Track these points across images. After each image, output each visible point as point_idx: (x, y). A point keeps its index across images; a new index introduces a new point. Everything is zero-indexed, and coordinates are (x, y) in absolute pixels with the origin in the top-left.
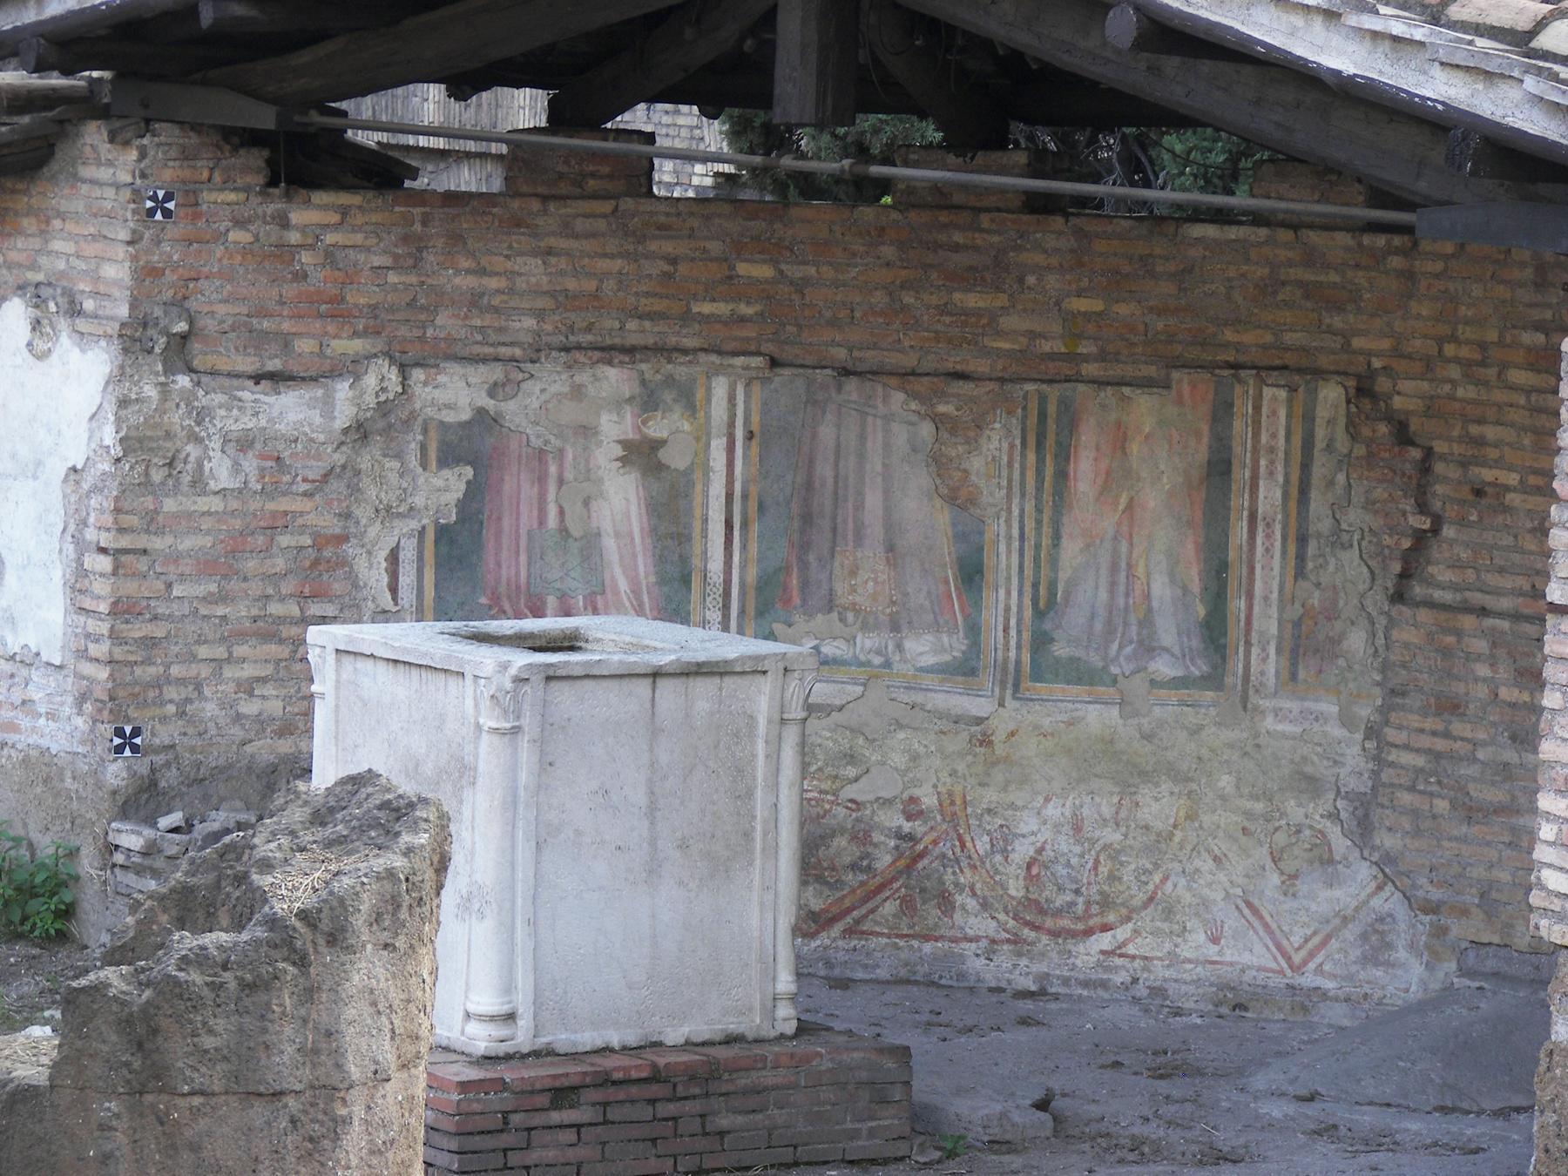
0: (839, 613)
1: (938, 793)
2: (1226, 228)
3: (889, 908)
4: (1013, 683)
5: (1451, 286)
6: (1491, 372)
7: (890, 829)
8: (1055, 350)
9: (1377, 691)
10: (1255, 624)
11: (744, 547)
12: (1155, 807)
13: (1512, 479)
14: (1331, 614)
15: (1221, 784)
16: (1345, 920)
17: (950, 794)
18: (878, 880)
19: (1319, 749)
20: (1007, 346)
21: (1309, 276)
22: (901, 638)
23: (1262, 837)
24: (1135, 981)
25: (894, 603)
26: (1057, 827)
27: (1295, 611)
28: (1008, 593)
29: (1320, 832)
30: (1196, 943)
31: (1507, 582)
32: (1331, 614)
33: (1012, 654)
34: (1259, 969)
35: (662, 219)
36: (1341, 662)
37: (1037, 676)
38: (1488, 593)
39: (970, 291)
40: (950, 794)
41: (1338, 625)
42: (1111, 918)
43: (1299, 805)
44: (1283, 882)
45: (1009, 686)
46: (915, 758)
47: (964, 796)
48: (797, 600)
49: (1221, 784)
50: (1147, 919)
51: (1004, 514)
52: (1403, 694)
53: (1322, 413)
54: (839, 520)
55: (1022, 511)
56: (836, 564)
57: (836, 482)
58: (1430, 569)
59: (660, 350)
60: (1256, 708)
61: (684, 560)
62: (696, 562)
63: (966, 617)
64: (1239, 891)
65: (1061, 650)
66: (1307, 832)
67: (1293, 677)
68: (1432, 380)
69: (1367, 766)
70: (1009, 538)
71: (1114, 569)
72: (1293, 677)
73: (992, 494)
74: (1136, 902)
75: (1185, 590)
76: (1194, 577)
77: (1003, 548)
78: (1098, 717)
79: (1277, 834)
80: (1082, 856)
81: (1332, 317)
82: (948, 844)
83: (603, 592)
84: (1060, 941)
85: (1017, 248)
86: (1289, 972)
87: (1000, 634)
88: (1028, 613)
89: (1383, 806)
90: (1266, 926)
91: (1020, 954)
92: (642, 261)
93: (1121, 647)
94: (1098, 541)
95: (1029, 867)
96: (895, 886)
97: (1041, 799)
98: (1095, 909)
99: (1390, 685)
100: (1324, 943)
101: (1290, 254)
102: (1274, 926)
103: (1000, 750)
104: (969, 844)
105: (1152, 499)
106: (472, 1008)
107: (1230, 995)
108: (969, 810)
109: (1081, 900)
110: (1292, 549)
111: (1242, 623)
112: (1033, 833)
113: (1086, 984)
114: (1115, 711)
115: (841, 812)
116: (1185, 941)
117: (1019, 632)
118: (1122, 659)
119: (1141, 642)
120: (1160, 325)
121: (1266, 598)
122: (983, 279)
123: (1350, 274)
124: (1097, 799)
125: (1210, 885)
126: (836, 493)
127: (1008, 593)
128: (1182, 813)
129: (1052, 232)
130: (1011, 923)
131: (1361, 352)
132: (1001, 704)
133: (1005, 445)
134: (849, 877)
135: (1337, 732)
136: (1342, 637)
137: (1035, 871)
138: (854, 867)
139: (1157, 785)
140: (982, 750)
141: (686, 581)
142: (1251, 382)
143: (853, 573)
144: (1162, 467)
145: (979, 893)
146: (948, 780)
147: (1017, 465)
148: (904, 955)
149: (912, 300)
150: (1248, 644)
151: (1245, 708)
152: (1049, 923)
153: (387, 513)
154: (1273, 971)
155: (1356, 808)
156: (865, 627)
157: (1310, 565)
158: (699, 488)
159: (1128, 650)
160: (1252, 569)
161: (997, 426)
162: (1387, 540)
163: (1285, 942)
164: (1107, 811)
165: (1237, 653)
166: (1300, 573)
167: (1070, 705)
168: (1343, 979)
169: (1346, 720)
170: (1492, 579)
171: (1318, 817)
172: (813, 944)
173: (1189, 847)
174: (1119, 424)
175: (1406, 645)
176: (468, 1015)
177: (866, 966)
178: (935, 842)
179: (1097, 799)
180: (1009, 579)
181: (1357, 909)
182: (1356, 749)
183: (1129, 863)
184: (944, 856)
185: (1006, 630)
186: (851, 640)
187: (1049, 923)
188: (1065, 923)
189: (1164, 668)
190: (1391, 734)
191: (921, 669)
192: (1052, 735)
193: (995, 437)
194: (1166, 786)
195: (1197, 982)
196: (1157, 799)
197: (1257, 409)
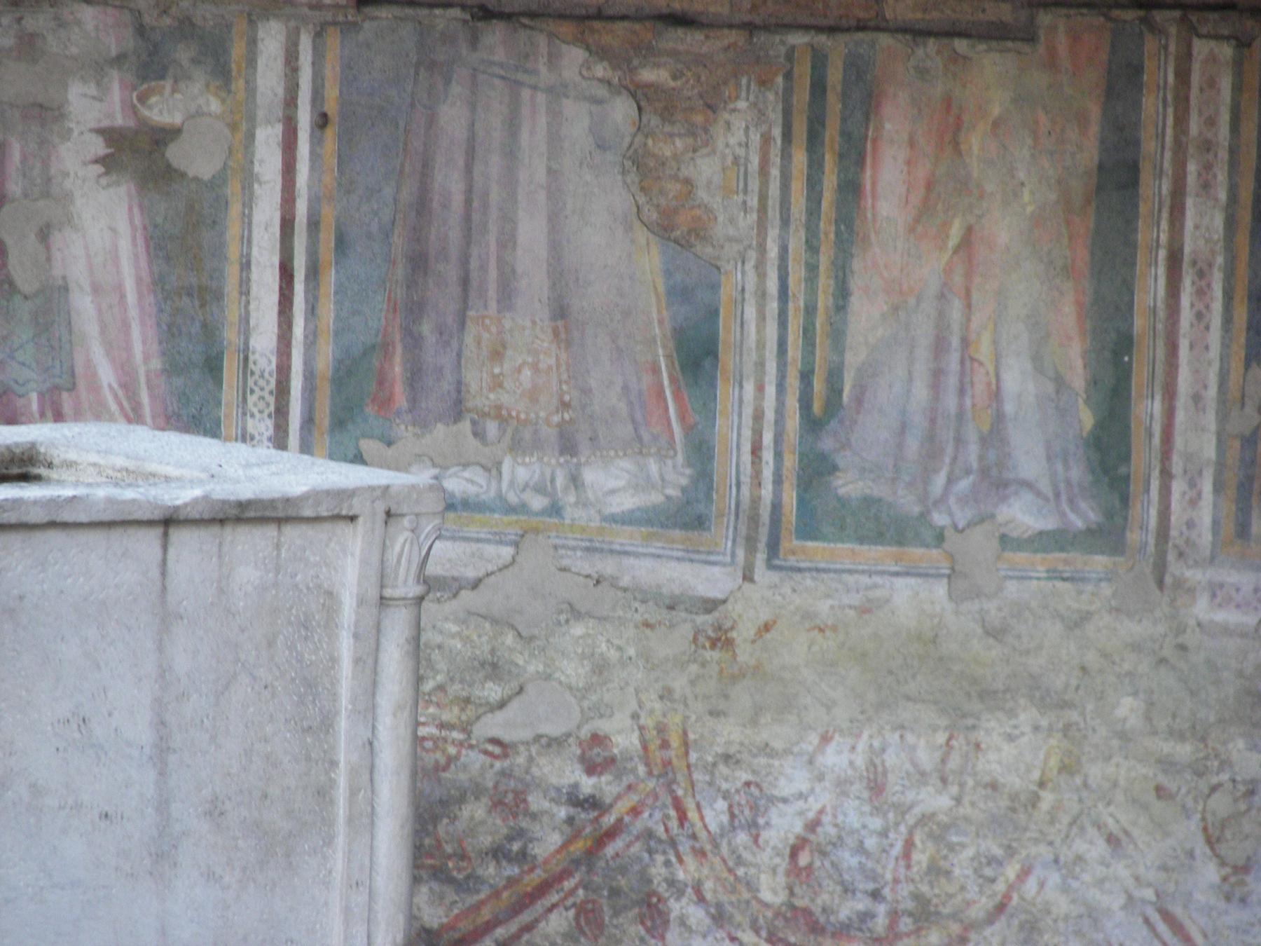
0: (474, 423)
1: (641, 728)
10: (1179, 442)
11: (312, 310)
12: (1008, 750)
15: (1121, 712)
17: (661, 729)
18: (538, 875)
22: (579, 465)
23: (1190, 802)
25: (565, 406)
26: (842, 786)
28: (760, 388)
33: (767, 492)
37: (808, 530)
40: (661, 729)
44: (1225, 879)
46: (601, 668)
47: (685, 733)
51: (752, 256)
54: (474, 264)
55: (784, 250)
56: (469, 339)
60: (1179, 584)
62: (230, 335)
63: (688, 429)
64: (1149, 894)
65: (848, 485)
70: (762, 295)
71: (940, 346)
72: (1243, 530)
73: (732, 221)
75: (1060, 383)
77: (750, 312)
80: (884, 834)
82: (658, 815)
83: (72, 388)
87: (747, 458)
88: (793, 422)
93: (950, 481)
95: (794, 853)
96: (568, 884)
97: (814, 738)
103: (745, 654)
104: (692, 815)
108: (693, 756)
109: (881, 909)
111: (1157, 440)
112: (801, 796)
115: (475, 760)
117: (778, 455)
118: (952, 500)
119: (984, 472)
124: (910, 739)
125: (1100, 882)
126: (467, 218)
127: (760, 388)
128: (1054, 762)
132: (748, 577)
133: (756, 138)
137: (804, 859)
138: (498, 853)
139: (1012, 713)
140: (717, 654)
141: (213, 367)
142: (1173, 30)
143: (497, 355)
144: (1022, 175)
145: (709, 896)
146: (658, 706)
147: (775, 172)
150: (1166, 475)
151: (1160, 583)
156: (516, 447)
158: (235, 209)
159: (964, 485)
160: (1173, 348)
161: (742, 104)
164: (927, 759)
165: (1148, 491)
167: (865, 580)
173: (1066, 820)
174: (948, 102)
178: (635, 811)
179: (910, 739)
180: (760, 365)
183: (963, 846)
184: (649, 834)
185: (756, 450)
186: (493, 468)
191: (613, 519)
192: (834, 629)
194: (1026, 717)
196: (1011, 738)
197: (1183, 76)
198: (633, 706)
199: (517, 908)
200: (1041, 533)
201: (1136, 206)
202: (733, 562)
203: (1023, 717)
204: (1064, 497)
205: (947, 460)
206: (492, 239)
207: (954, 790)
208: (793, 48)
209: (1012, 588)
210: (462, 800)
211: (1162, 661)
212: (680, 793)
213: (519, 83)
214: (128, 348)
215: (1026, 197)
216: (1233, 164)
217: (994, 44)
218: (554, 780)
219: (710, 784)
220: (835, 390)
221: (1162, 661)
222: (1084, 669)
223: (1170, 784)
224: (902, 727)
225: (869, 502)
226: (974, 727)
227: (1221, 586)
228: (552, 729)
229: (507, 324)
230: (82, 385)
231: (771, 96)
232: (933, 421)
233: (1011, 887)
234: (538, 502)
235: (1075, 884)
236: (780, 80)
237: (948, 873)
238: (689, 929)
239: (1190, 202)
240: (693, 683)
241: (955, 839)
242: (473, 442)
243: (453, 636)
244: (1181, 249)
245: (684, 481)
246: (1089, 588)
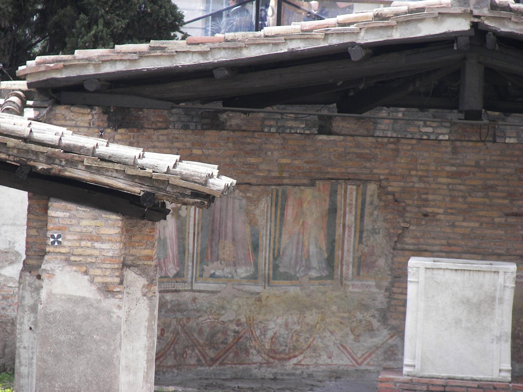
0: (220, 261)
1: (246, 317)
2: (330, 136)
3: (231, 355)
4: (268, 281)
5: (414, 154)
6: (431, 179)
7: (232, 330)
8: (276, 175)
9: (390, 277)
10: (345, 259)
11: (197, 241)
12: (311, 317)
13: (441, 211)
14: (372, 254)
15: (332, 309)
16: (377, 348)
17: (249, 317)
18: (229, 346)
19: (367, 296)
20: (262, 174)
21: (358, 151)
22: (236, 269)
23: (348, 325)
24: (302, 373)
25: (234, 257)
26: (280, 326)
27: (359, 254)
28: (266, 253)
29: (369, 321)
30: (324, 359)
31: (438, 242)
32: (372, 254)
33: (267, 272)
34: (345, 366)
35: (176, 135)
36: (376, 269)
37: (274, 279)
38: (429, 245)
39: (252, 157)
40: (249, 317)
41: (374, 258)
42: (297, 353)
43: (361, 313)
44: (355, 338)
45: (267, 282)
46: (240, 307)
47: (253, 318)
48: (209, 258)
49: (332, 309)
50: (308, 353)
51: (265, 228)
52: (399, 277)
53: (369, 193)
54: (221, 231)
55: (271, 226)
56: (220, 245)
57: (220, 219)
58: (404, 239)
60: (346, 285)
61: (184, 246)
62: (187, 247)
63: (254, 261)
64: (339, 342)
65: (282, 270)
66: (364, 322)
67: (358, 274)
68: (404, 182)
69: (385, 300)
70: (266, 235)
71: (298, 243)
72: (358, 274)
73: (262, 221)
74: (304, 348)
75: (321, 249)
76: (324, 245)
77: (264, 238)
78: (293, 290)
79: (353, 323)
80: (288, 334)
81: (366, 163)
82: (248, 334)
83: (167, 258)
84: (281, 362)
85: (266, 143)
86: (357, 366)
87: (263, 266)
88: (271, 259)
89: (392, 312)
90: (348, 352)
91: (269, 367)
92: (173, 149)
93: (300, 268)
94: (293, 235)
95: (272, 339)
96: (233, 348)
97: (276, 317)
98: (292, 351)
99: (394, 275)
100: (370, 355)
101: (351, 144)
102: (351, 352)
103: (264, 302)
104: (254, 333)
105: (310, 221)
106: (502, 368)
107: (334, 374)
108: (255, 322)
109: (287, 348)
110: (358, 235)
111: (340, 258)
112: (273, 328)
113: (288, 375)
114: (298, 288)
115: (219, 325)
116: (320, 358)
117: (269, 265)
118: (300, 272)
119: (306, 266)
120: (308, 167)
121: (348, 251)
122: (255, 153)
123: (373, 150)
124: (293, 316)
125: (329, 341)
126: (220, 223)
127: (266, 253)
128: (320, 319)
129: (276, 138)
130: (266, 357)
131: (376, 174)
132: (265, 288)
133: (266, 206)
134: (221, 346)
135: (375, 290)
136: (376, 261)
137: (273, 340)
138: (222, 343)
139: (311, 310)
140: (259, 303)
141: (184, 253)
142: (343, 184)
143: (224, 248)
144: (313, 211)
145: (257, 348)
146: (249, 313)
147: (269, 212)
148: (234, 370)
149: (236, 160)
150: (342, 265)
151: (342, 285)
152: (278, 356)
154: (351, 366)
155: (381, 313)
156: (227, 266)
157: (364, 239)
158: (188, 223)
159: (302, 269)
160: (343, 242)
161: (264, 200)
162: (392, 231)
163: (355, 356)
164: (296, 320)
165: (338, 268)
166: (360, 242)
167: (285, 287)
168: (377, 366)
169: (378, 286)
170: (431, 241)
171: (368, 317)
172: (212, 368)
173: (322, 329)
174: (300, 198)
175: (400, 263)
176: (500, 371)
177: (224, 375)
178: (244, 333)
179: (293, 316)
180: (266, 248)
181: (382, 344)
182: (382, 295)
183: (302, 336)
184: (247, 337)
185: (265, 264)
186: (223, 270)
187: (278, 356)
188: (283, 356)
189: (313, 274)
190: (395, 290)
191: (242, 278)
192: (280, 296)
193: (263, 203)
194: (314, 311)
195: (323, 371)
196: (311, 315)
197: (346, 192)
198: (245, 313)
199: (225, 353)
200: (317, 277)
201: (336, 216)
202: (262, 285)
203: (314, 311)
204: (321, 270)
205: (299, 264)
206: (223, 226)
207: (301, 325)
208: (272, 189)
209: (311, 287)
210: (217, 333)
211: (342, 299)
212: (252, 329)
213: (228, 197)
214: (174, 250)
215: (314, 215)
216: (356, 208)
217: (308, 187)
218: (231, 328)
219: (257, 327)
220: (279, 252)
221: (342, 299)
222: (326, 301)
223: (343, 321)
224: (291, 314)
225: (285, 273)
226: (304, 313)
227: (354, 284)
228: (231, 319)
229: (225, 242)
230: (168, 257)
231: (269, 198)
232: (297, 257)
233: (311, 342)
234: (230, 276)
235: (323, 341)
236: (270, 195)
237: (299, 341)
238: (253, 355)
239: (347, 215)
240: (255, 308)
241: (301, 334)
242: (220, 265)
243: (216, 302)
244: (345, 224)
245: (253, 271)
246: (327, 286)
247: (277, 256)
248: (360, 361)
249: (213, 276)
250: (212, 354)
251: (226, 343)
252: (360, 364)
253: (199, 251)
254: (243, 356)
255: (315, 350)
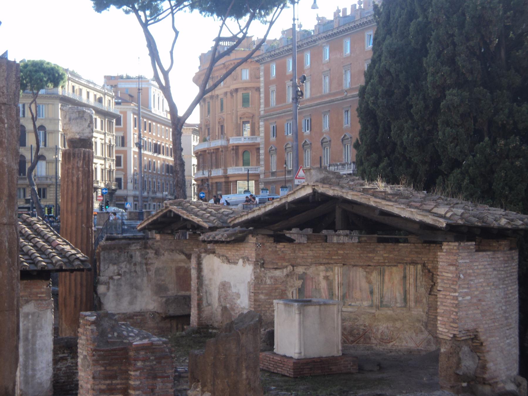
4: (378, 308)
37: (381, 307)
42: (393, 340)
53: (418, 269)
59: (328, 263)
65: (384, 303)
67: (416, 306)
72: (416, 306)
76: (402, 292)
88: (380, 298)
103: (377, 317)
105: (396, 282)
110: (415, 288)
141: (333, 295)
153: (291, 287)
166: (416, 291)
187: (384, 341)
188: (386, 341)
189: (398, 305)
194: (399, 322)
197: (410, 269)
247: (382, 297)
248: (418, 345)
249: (350, 305)
250: (351, 339)
251: (359, 334)
252: (418, 347)
253: (342, 295)
254: (368, 340)
255: (400, 339)
